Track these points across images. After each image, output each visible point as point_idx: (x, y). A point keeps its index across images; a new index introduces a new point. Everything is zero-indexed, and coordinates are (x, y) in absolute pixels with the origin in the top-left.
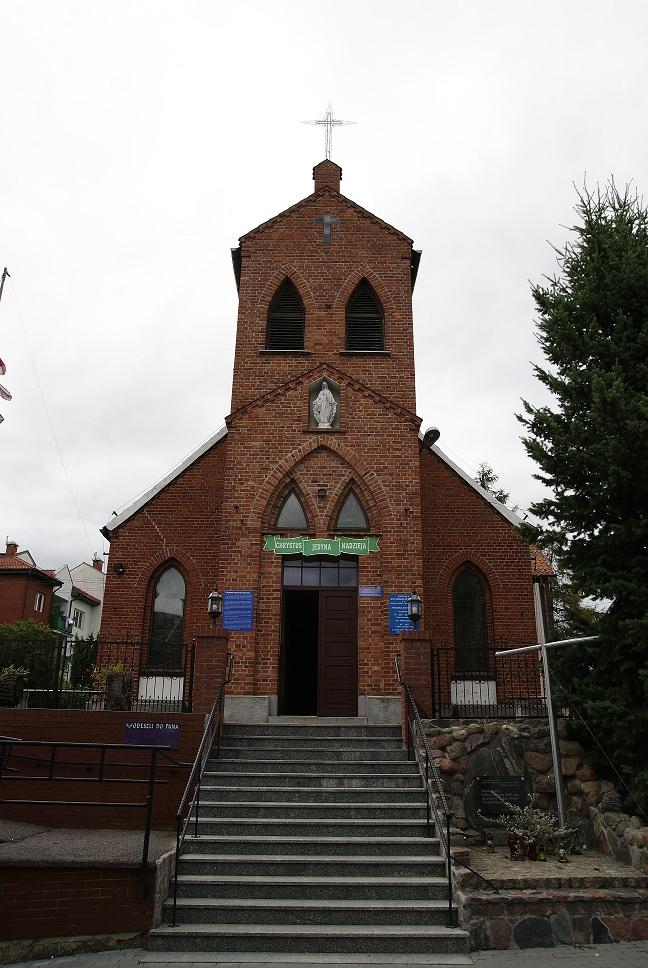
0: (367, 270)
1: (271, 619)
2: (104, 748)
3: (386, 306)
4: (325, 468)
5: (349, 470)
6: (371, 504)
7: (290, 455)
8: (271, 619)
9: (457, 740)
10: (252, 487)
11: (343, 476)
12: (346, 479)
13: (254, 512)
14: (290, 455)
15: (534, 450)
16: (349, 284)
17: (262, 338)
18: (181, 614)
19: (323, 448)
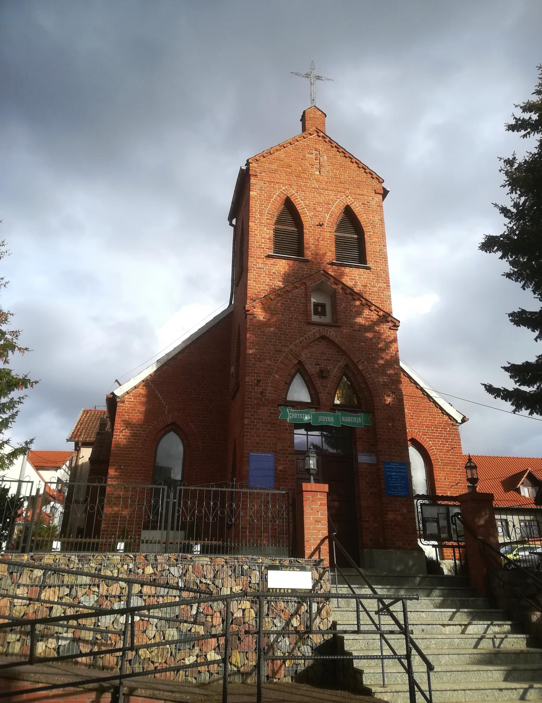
0: (349, 201)
1: (287, 479)
2: (338, 607)
3: (365, 229)
4: (325, 354)
5: (344, 358)
6: (363, 385)
7: (298, 341)
8: (287, 479)
9: (50, 612)
10: (269, 365)
11: (339, 361)
12: (341, 364)
13: (271, 386)
14: (298, 341)
15: (511, 321)
16: (337, 209)
17: (270, 244)
18: (298, 374)
19: (323, 337)
